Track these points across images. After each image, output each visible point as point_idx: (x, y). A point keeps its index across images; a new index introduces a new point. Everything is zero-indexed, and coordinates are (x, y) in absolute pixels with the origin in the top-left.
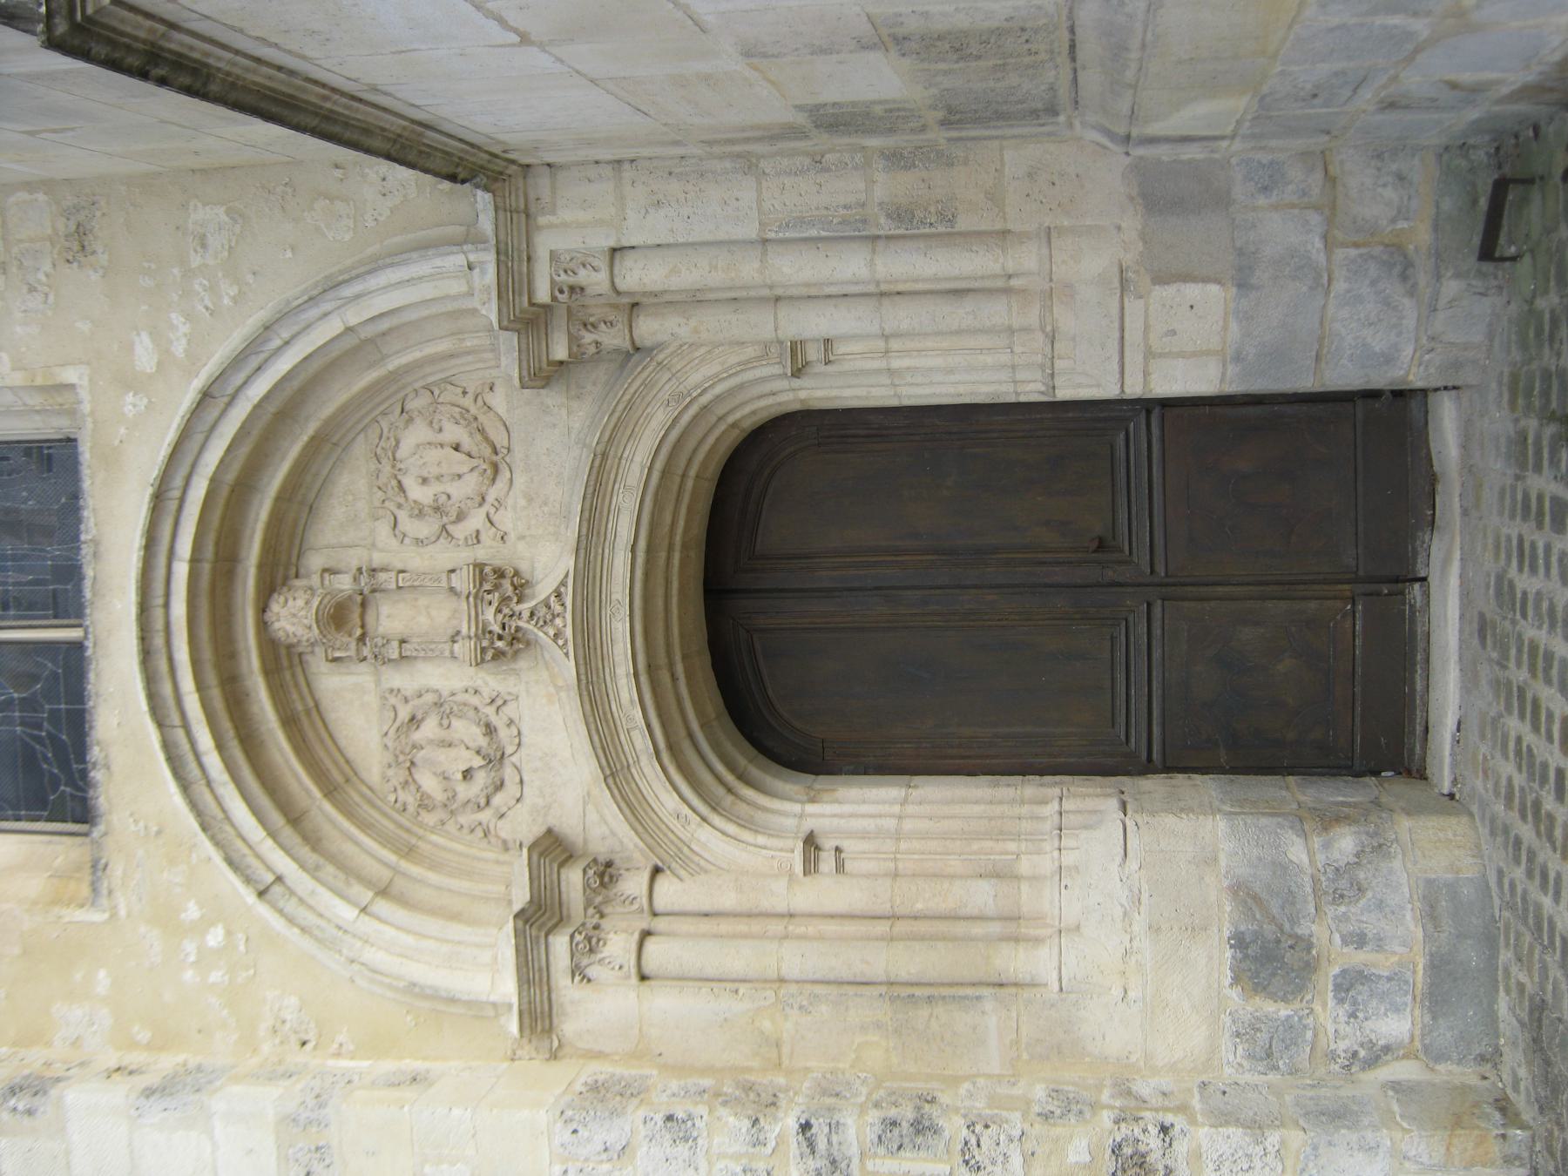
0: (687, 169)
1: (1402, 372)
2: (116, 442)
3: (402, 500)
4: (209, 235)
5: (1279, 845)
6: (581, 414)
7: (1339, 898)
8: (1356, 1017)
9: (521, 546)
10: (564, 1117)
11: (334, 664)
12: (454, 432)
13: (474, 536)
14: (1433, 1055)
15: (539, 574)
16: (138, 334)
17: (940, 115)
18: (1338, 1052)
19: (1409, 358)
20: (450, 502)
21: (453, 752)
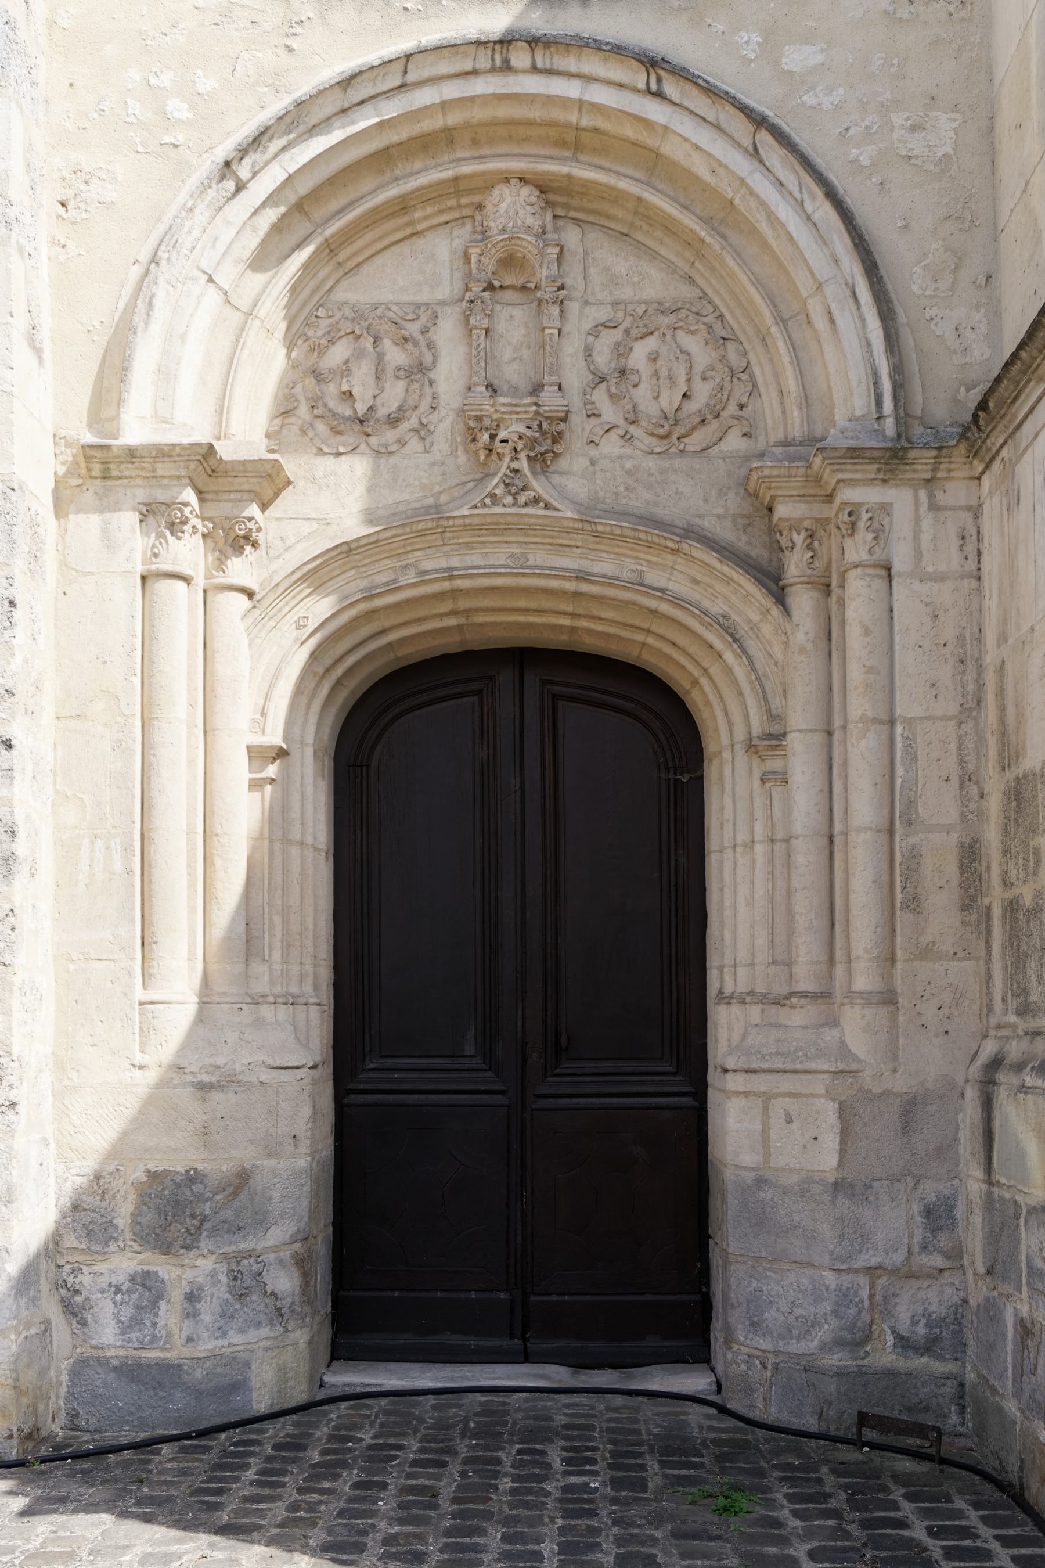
0: (968, 646)
1: (742, 1339)
2: (708, 21)
3: (634, 333)
4: (924, 133)
5: (282, 1218)
6: (718, 528)
7: (235, 1276)
8: (116, 1293)
9: (584, 462)
10: (9, 491)
11: (462, 254)
12: (702, 393)
13: (596, 412)
14: (81, 1367)
15: (556, 479)
16: (822, 51)
17: (1028, 901)
18: (80, 1275)
19: (755, 1345)
20: (630, 387)
21: (371, 381)
